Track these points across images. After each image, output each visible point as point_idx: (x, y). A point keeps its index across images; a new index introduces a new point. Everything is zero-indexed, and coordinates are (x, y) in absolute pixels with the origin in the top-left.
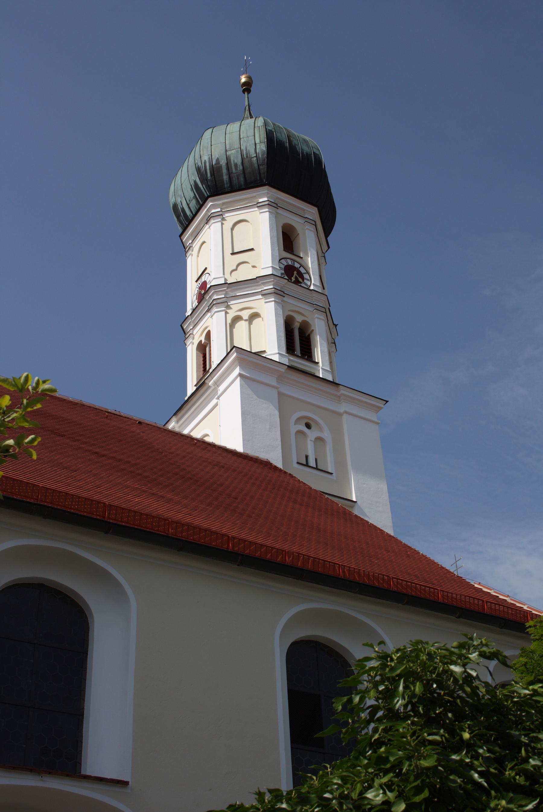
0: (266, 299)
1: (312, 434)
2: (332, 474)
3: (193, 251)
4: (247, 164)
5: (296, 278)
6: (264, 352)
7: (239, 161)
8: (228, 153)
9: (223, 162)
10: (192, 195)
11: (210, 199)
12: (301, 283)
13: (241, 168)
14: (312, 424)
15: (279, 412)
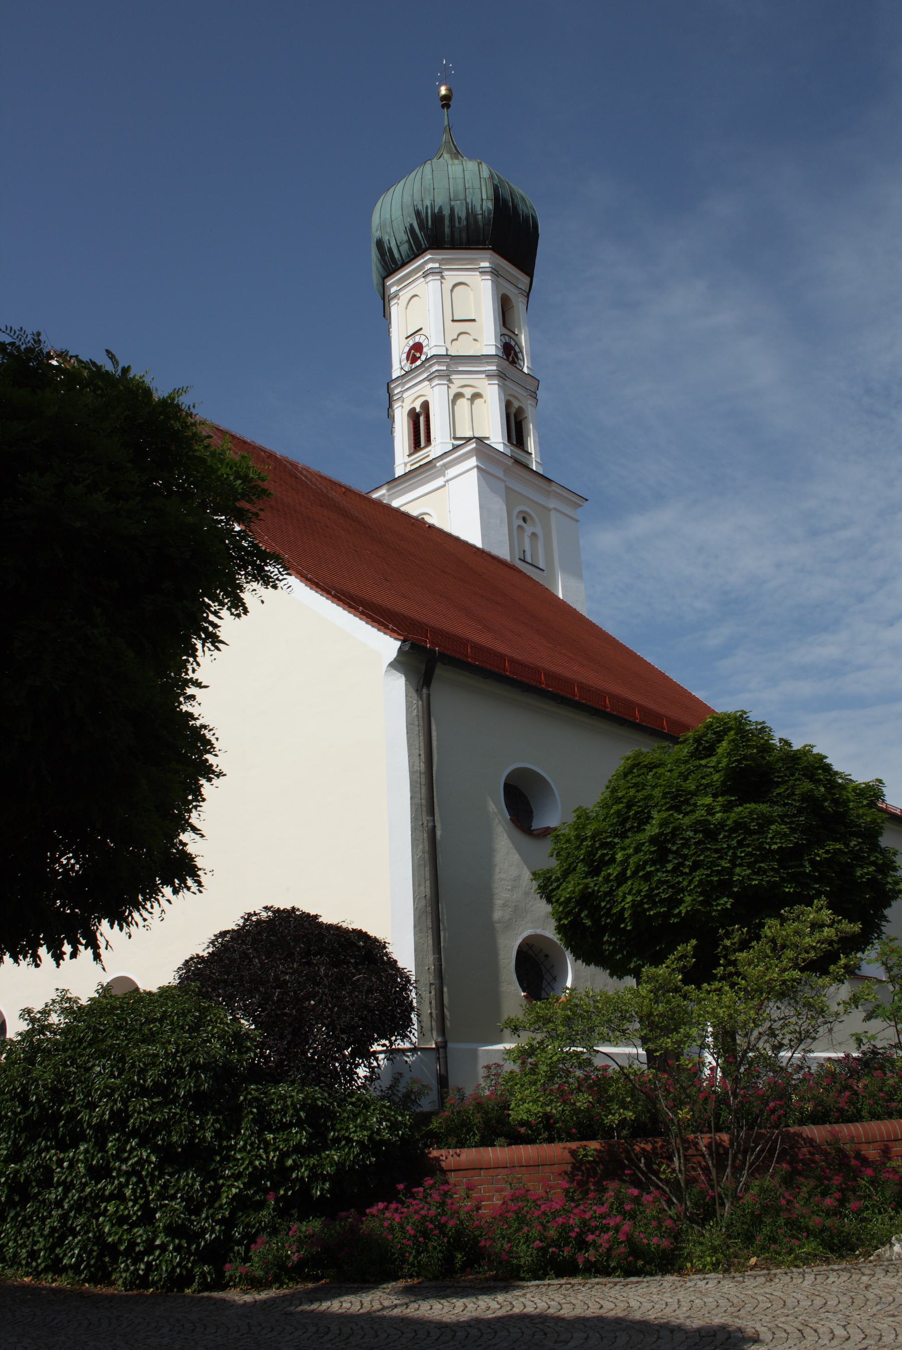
0: (489, 380)
1: (529, 529)
2: (543, 570)
3: (399, 299)
4: (472, 220)
5: (513, 358)
6: (488, 438)
7: (463, 215)
8: (453, 203)
9: (446, 212)
10: (405, 238)
11: (429, 251)
12: (516, 363)
13: (465, 223)
14: (528, 518)
15: (507, 505)
